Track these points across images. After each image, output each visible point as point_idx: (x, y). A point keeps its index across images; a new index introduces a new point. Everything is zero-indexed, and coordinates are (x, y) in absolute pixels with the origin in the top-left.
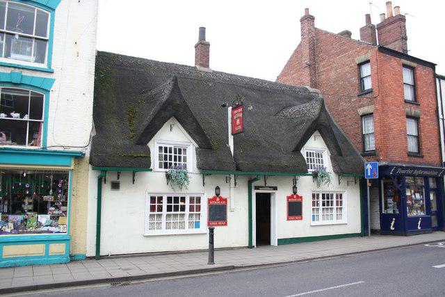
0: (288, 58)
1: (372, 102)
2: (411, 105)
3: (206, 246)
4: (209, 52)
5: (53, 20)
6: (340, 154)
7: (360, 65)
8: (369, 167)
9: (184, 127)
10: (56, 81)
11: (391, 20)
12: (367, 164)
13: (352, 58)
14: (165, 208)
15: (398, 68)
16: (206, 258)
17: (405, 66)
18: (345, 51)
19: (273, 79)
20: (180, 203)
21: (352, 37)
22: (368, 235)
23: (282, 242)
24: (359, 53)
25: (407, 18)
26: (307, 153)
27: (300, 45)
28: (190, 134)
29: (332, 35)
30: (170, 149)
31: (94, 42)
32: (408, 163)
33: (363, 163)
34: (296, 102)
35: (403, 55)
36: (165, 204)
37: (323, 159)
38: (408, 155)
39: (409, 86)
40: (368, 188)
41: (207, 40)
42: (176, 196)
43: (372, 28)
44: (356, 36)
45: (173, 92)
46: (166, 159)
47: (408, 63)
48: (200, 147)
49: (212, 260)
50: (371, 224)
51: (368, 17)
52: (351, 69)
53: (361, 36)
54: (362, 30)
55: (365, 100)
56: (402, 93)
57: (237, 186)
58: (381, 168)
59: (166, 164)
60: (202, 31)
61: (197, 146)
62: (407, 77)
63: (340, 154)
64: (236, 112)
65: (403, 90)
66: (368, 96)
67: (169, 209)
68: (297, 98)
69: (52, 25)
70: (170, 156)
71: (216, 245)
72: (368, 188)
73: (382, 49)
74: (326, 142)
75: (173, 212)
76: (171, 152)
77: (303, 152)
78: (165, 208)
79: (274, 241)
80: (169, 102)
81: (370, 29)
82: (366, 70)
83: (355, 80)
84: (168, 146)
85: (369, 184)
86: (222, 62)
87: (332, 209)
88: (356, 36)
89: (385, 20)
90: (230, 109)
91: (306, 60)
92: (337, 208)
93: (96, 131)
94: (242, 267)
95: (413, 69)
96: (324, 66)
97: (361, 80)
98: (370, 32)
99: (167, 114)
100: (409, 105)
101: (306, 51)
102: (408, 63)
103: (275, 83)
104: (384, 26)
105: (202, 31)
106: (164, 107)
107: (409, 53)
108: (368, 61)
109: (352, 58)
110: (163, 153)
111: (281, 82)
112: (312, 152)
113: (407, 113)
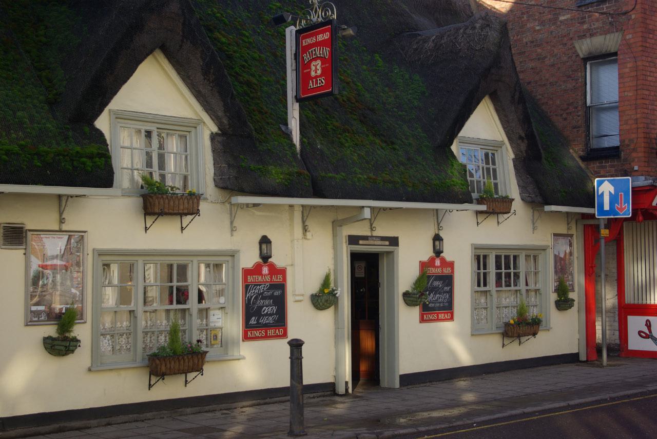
37: (498, 181)
78: (492, 278)
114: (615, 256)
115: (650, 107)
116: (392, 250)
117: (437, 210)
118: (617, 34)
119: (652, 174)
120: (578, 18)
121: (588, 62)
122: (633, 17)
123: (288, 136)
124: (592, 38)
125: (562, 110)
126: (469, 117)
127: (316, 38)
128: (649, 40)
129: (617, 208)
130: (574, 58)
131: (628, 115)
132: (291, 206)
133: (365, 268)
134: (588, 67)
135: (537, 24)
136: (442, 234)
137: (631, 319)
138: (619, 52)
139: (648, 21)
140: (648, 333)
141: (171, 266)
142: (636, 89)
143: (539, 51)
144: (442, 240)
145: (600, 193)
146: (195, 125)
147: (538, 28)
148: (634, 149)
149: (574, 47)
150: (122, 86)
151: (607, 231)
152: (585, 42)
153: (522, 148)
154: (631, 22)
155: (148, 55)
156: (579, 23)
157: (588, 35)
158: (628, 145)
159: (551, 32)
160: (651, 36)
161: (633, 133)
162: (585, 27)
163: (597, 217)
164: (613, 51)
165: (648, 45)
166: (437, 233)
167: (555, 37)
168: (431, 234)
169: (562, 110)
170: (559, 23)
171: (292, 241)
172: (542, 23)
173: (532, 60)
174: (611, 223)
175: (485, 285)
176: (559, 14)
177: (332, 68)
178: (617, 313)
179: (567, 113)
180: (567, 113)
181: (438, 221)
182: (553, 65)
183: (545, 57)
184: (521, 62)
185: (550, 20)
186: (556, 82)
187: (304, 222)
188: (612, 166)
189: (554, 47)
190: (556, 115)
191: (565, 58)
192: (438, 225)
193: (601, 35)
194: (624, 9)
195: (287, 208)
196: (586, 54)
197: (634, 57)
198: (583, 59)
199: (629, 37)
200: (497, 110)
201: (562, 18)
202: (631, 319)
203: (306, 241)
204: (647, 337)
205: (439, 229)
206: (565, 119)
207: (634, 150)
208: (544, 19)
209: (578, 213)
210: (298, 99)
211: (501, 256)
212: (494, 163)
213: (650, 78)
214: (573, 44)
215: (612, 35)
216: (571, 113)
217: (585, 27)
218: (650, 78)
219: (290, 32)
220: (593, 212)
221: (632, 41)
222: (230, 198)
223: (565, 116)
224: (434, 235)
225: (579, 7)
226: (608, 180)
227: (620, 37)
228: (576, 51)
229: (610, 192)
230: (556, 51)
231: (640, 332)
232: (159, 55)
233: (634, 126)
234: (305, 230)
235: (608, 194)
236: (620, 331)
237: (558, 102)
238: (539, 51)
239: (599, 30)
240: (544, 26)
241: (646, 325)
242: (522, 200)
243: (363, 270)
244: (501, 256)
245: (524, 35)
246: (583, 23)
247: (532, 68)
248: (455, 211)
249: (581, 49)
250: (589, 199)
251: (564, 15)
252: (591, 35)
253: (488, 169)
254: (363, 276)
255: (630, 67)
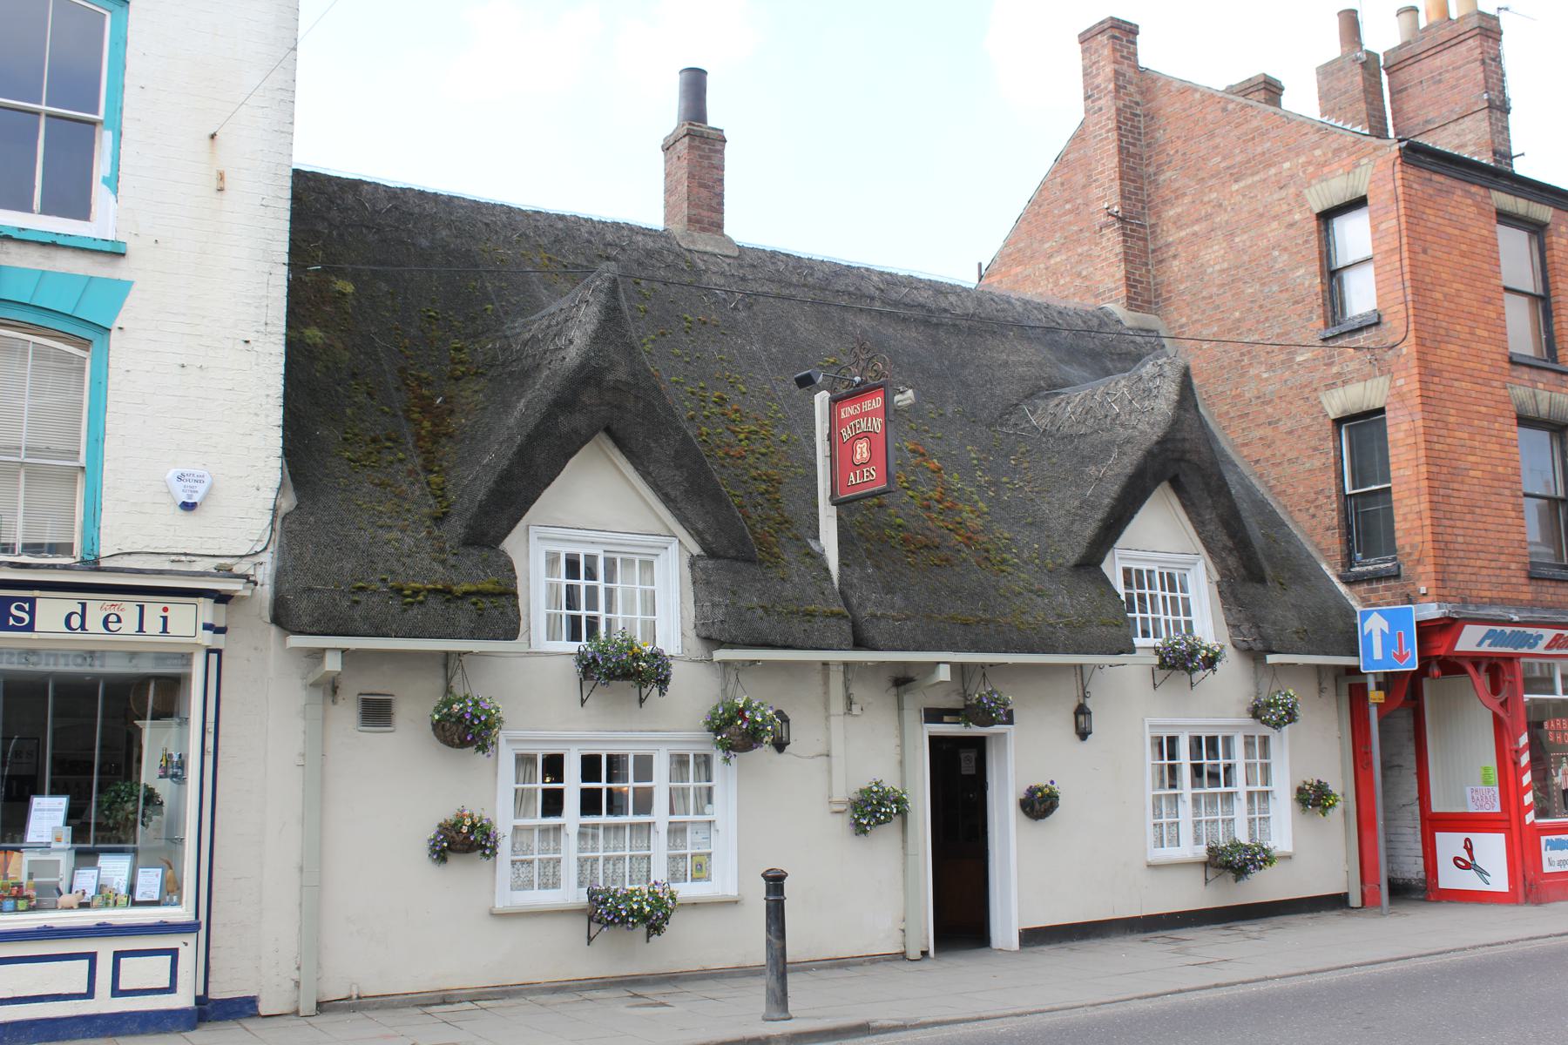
0: (1029, 189)
1: (1378, 363)
2: (1535, 374)
3: (755, 950)
4: (721, 168)
5: (121, 42)
6: (1254, 574)
7: (1327, 217)
8: (1374, 626)
9: (645, 475)
10: (134, 289)
11: (1445, 34)
12: (1365, 616)
13: (1292, 190)
14: (572, 801)
15: (1481, 226)
16: (756, 994)
17: (1505, 217)
18: (1267, 161)
19: (969, 280)
20: (629, 786)
21: (1287, 102)
22: (1378, 904)
23: (1033, 937)
24: (1320, 169)
25: (1506, 22)
26: (1127, 572)
27: (1079, 138)
28: (667, 500)
29: (1209, 96)
30: (591, 559)
31: (285, 130)
32: (1531, 605)
33: (1349, 613)
34: (1073, 371)
35: (1499, 175)
36: (572, 785)
37: (1193, 618)
38: (1531, 578)
39: (1525, 300)
40: (1374, 713)
41: (713, 120)
42: (616, 750)
43: (1370, 65)
44: (1302, 99)
45: (599, 338)
46: (572, 603)
47: (1520, 205)
48: (710, 553)
49: (780, 999)
50: (1390, 858)
51: (1351, 22)
52: (1291, 232)
53: (1324, 96)
54: (1327, 72)
55: (1348, 357)
56: (1498, 326)
57: (856, 709)
58: (1426, 630)
59: (575, 622)
60: (695, 83)
61: (696, 549)
62: (1514, 249)
63: (1254, 574)
64: (847, 411)
65: (1501, 315)
66: (1361, 339)
67: (590, 803)
68: (1074, 354)
69: (120, 66)
70: (592, 592)
71: (795, 950)
72: (1374, 713)
73: (1416, 155)
74: (1199, 525)
75: (604, 819)
76: (591, 575)
77: (1114, 567)
78: (572, 801)
79: (1006, 922)
80: (587, 376)
81: (1358, 69)
82: (1354, 235)
83: (1309, 278)
84: (582, 551)
85: (1376, 696)
86: (287, 261)
87: (1229, 797)
88: (1302, 99)
89: (1416, 34)
90: (821, 399)
91: (1107, 195)
92: (1250, 795)
93: (296, 489)
94: (904, 1028)
95: (1537, 229)
96: (1178, 223)
97: (1333, 276)
98: (1359, 79)
99: (580, 421)
100: (1526, 374)
101: (1108, 164)
102: (1520, 205)
103: (977, 296)
104: (1415, 58)
105: (695, 83)
106: (565, 401)
107: (1520, 168)
108: (1359, 203)
109: (1292, 190)
110: (564, 581)
111: (1000, 286)
112: (1144, 567)
113: (1520, 405)
114: (1412, 734)
115: (1442, 492)
116: (1003, 731)
117: (1081, 666)
118: (1382, 379)
119: (1450, 599)
120: (1323, 358)
121: (1344, 426)
122: (1405, 351)
123: (818, 558)
124: (1347, 387)
125: (1307, 501)
126: (1133, 517)
127: (861, 407)
128: (1432, 387)
129: (1395, 655)
130: (1321, 419)
131: (1407, 506)
132: (825, 664)
133: (976, 759)
134: (1343, 432)
135: (1263, 369)
136: (1090, 704)
137: (1440, 837)
138: (1387, 408)
139: (1429, 358)
140: (1468, 860)
141: (1199, 739)
142: (1415, 463)
143: (1269, 410)
144: (1090, 713)
145: (1366, 631)
146: (666, 545)
147: (1265, 375)
148: (1418, 560)
149: (1320, 402)
150: (542, 491)
151: (1381, 694)
152: (1336, 394)
153: (1230, 563)
154: (1402, 360)
155: (583, 443)
156: (1325, 365)
157: (1339, 382)
158: (1410, 554)
159: (1286, 381)
160: (1436, 380)
161: (1416, 534)
162: (1335, 370)
163: (1363, 671)
164: (1377, 406)
165: (1431, 394)
166: (1082, 701)
167: (1291, 388)
168: (1073, 705)
169: (1307, 501)
170: (1296, 367)
171: (827, 718)
172: (1271, 367)
173: (1259, 425)
174: (1390, 681)
175: (1173, 786)
176: (1295, 353)
177: (884, 449)
178: (1419, 827)
179: (1316, 507)
180: (1316, 507)
181: (1083, 684)
182: (1291, 432)
183: (1279, 420)
184: (1243, 429)
185: (1283, 362)
186: (1297, 458)
187: (847, 688)
188: (1387, 589)
189: (1291, 403)
190: (1300, 510)
191: (1308, 421)
192: (1084, 690)
193: (1358, 381)
194: (1390, 342)
195: (819, 667)
196: (1338, 412)
197: (1410, 414)
198: (1334, 420)
199: (1400, 382)
200: (1184, 506)
201: (1299, 359)
202: (1440, 837)
203: (849, 718)
204: (1468, 867)
205: (1085, 696)
206: (1314, 516)
207: (1419, 562)
208: (1273, 361)
209: (1336, 667)
210: (835, 502)
211: (599, 757)
212: (1184, 590)
213: (1437, 446)
214: (1318, 398)
215: (1375, 381)
216: (1321, 506)
217: (1335, 370)
218: (1437, 446)
219: (821, 399)
220: (1356, 664)
221: (1405, 389)
222: (710, 653)
223: (1312, 511)
224: (1076, 704)
225: (1325, 340)
226: (1379, 612)
227: (1388, 383)
228: (1323, 408)
229: (1382, 631)
230: (1294, 410)
231: (1456, 859)
232: (603, 441)
233: (1417, 523)
234: (850, 702)
235: (1379, 633)
236: (1425, 857)
237: (1301, 490)
238: (1269, 410)
239: (1355, 375)
240: (1274, 371)
241: (1465, 847)
242: (1235, 646)
243: (973, 763)
244: (599, 757)
245: (1246, 388)
246: (1330, 365)
247: (1261, 439)
248: (1107, 667)
249: (1330, 405)
250: (1349, 641)
251: (1302, 354)
252: (1345, 383)
253: (1174, 600)
254: (974, 772)
255: (1406, 430)
